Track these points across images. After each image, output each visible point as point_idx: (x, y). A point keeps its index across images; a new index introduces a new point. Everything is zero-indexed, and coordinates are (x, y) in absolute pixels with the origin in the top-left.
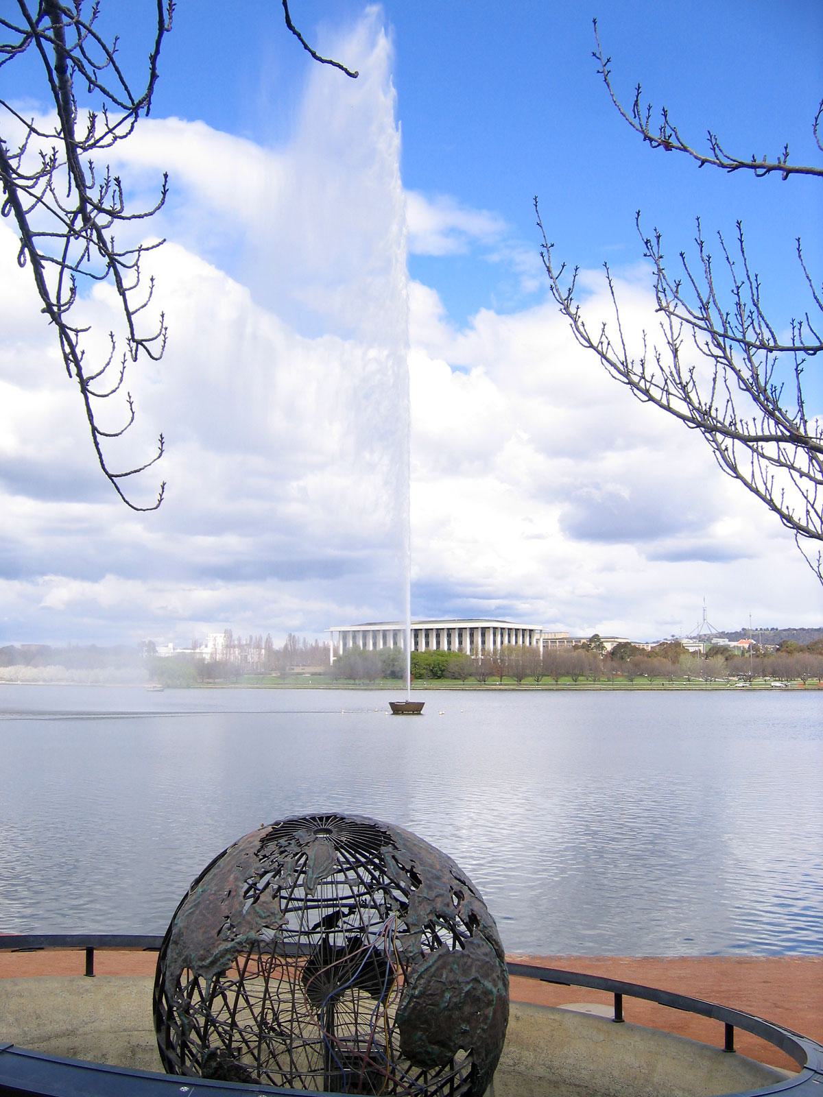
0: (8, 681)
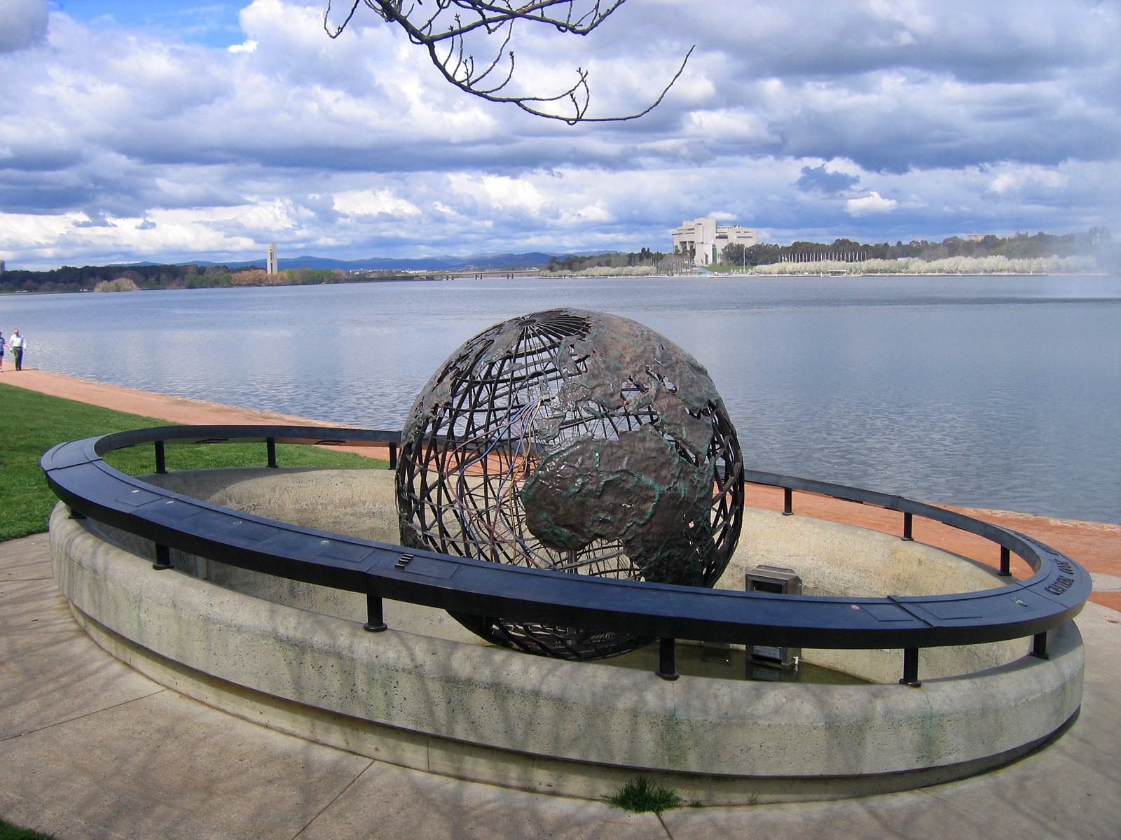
0: (949, 273)
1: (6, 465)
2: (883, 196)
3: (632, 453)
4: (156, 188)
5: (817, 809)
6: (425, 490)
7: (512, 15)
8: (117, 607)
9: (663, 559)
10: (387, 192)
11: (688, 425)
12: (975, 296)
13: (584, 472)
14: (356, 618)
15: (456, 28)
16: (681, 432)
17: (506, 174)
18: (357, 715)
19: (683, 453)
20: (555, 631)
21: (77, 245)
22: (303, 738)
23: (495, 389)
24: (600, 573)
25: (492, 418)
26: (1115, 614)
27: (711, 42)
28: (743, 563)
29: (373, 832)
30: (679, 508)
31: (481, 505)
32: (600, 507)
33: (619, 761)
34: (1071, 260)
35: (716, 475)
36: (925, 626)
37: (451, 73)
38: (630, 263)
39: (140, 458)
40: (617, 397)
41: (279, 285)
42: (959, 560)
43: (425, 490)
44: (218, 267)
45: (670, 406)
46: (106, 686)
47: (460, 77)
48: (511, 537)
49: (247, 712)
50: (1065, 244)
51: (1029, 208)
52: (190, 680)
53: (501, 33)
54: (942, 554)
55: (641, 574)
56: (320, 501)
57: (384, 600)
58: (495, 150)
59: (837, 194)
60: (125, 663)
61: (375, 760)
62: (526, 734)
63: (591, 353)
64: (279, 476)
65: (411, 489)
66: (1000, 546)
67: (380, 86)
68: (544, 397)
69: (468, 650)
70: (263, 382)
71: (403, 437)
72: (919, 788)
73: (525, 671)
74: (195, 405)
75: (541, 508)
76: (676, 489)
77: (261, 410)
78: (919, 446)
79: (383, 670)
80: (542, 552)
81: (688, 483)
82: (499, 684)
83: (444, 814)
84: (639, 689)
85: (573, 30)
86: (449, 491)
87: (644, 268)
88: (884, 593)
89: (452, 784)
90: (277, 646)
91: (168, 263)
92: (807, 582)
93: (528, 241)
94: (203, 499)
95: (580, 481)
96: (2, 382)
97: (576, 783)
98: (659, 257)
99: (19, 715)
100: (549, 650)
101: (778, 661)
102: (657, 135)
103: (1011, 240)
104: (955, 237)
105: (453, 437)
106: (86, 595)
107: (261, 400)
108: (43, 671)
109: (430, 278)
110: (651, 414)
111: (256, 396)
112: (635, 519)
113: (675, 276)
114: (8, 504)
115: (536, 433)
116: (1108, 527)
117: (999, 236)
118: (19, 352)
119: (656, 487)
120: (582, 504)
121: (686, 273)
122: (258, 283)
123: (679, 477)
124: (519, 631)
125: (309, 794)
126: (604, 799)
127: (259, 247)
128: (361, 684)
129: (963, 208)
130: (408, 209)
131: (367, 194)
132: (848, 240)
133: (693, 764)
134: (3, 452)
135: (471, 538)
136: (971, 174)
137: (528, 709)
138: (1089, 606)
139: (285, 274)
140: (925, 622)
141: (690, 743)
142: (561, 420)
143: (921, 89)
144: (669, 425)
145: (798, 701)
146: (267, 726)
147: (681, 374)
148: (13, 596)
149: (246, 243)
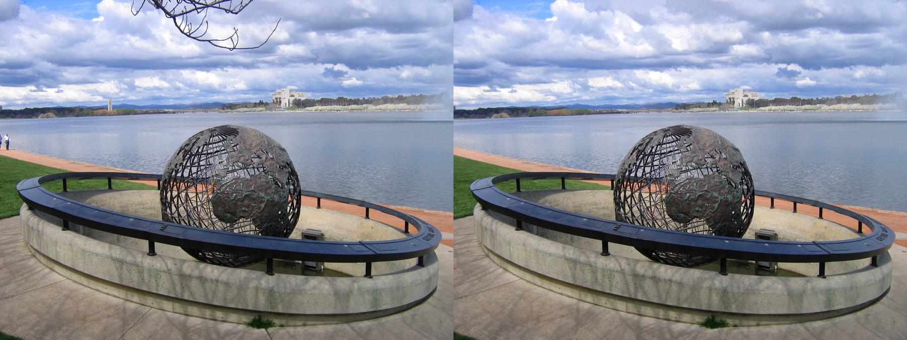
1: (2, 188)
2: (357, 79)
3: (256, 183)
4: (517, 76)
5: (330, 328)
6: (172, 198)
7: (207, 6)
8: (501, 246)
9: (722, 227)
10: (610, 78)
11: (731, 172)
12: (394, 120)
13: (690, 191)
14: (144, 250)
15: (185, 11)
16: (275, 175)
17: (205, 71)
18: (598, 290)
19: (730, 183)
20: (225, 255)
21: (484, 99)
22: (576, 299)
23: (654, 158)
24: (243, 232)
25: (653, 169)
26: (905, 249)
27: (740, 17)
28: (300, 228)
29: (151, 337)
30: (275, 206)
31: (195, 205)
32: (696, 205)
33: (704, 308)
34: (887, 105)
35: (290, 193)
36: (828, 253)
37: (183, 30)
38: (255, 107)
39: (57, 185)
40: (703, 161)
41: (567, 115)
42: (842, 227)
43: (172, 198)
44: (88, 108)
45: (271, 164)
46: (497, 277)
47: (186, 31)
48: (660, 217)
49: (100, 288)
50: (431, 99)
51: (416, 84)
52: (530, 275)
53: (203, 14)
54: (381, 224)
55: (259, 232)
56: (130, 203)
57: (156, 243)
58: (654, 61)
59: (792, 79)
60: (51, 268)
61: (152, 307)
62: (666, 297)
63: (693, 143)
64: (113, 193)
65: (620, 198)
66: (858, 221)
67: (607, 35)
68: (220, 161)
69: (643, 263)
70: (106, 155)
71: (616, 177)
72: (825, 319)
73: (666, 272)
74: (533, 164)
75: (672, 206)
76: (273, 198)
77: (106, 166)
78: (372, 180)
79: (609, 272)
80: (219, 223)
81: (732, 196)
82: (202, 277)
83: (180, 330)
84: (259, 279)
85: (232, 12)
86: (635, 199)
87: (261, 109)
88: (811, 240)
89: (636, 317)
90: (112, 261)
91: (521, 106)
92: (327, 236)
93: (214, 98)
94: (536, 202)
95: (234, 194)
96: (1, 154)
97: (687, 317)
98: (267, 104)
99: (8, 289)
100: (675, 263)
101: (315, 268)
102: (266, 55)
103: (409, 97)
104: (840, 96)
105: (184, 177)
106: (35, 241)
107: (559, 162)
108: (17, 272)
109: (627, 113)
110: (717, 167)
111: (104, 160)
112: (710, 210)
113: (727, 112)
114: (3, 204)
115: (217, 175)
116: (902, 213)
117: (858, 96)
118: (8, 142)
119: (719, 197)
120: (235, 204)
121: (278, 111)
122: (105, 114)
123: (275, 193)
124: (663, 255)
125: (125, 322)
126: (698, 323)
127: (105, 100)
128: (599, 277)
129: (390, 84)
130: (165, 85)
131: (149, 78)
132: (796, 98)
133: (734, 309)
134: (1, 183)
135: (190, 218)
136: (847, 70)
137: (214, 287)
138: (441, 245)
139: (115, 111)
140: (375, 252)
141: (733, 301)
142: (227, 170)
143: (373, 36)
144: (271, 172)
145: (323, 284)
146: (561, 294)
147: (729, 151)
148: (459, 241)
149: (100, 98)
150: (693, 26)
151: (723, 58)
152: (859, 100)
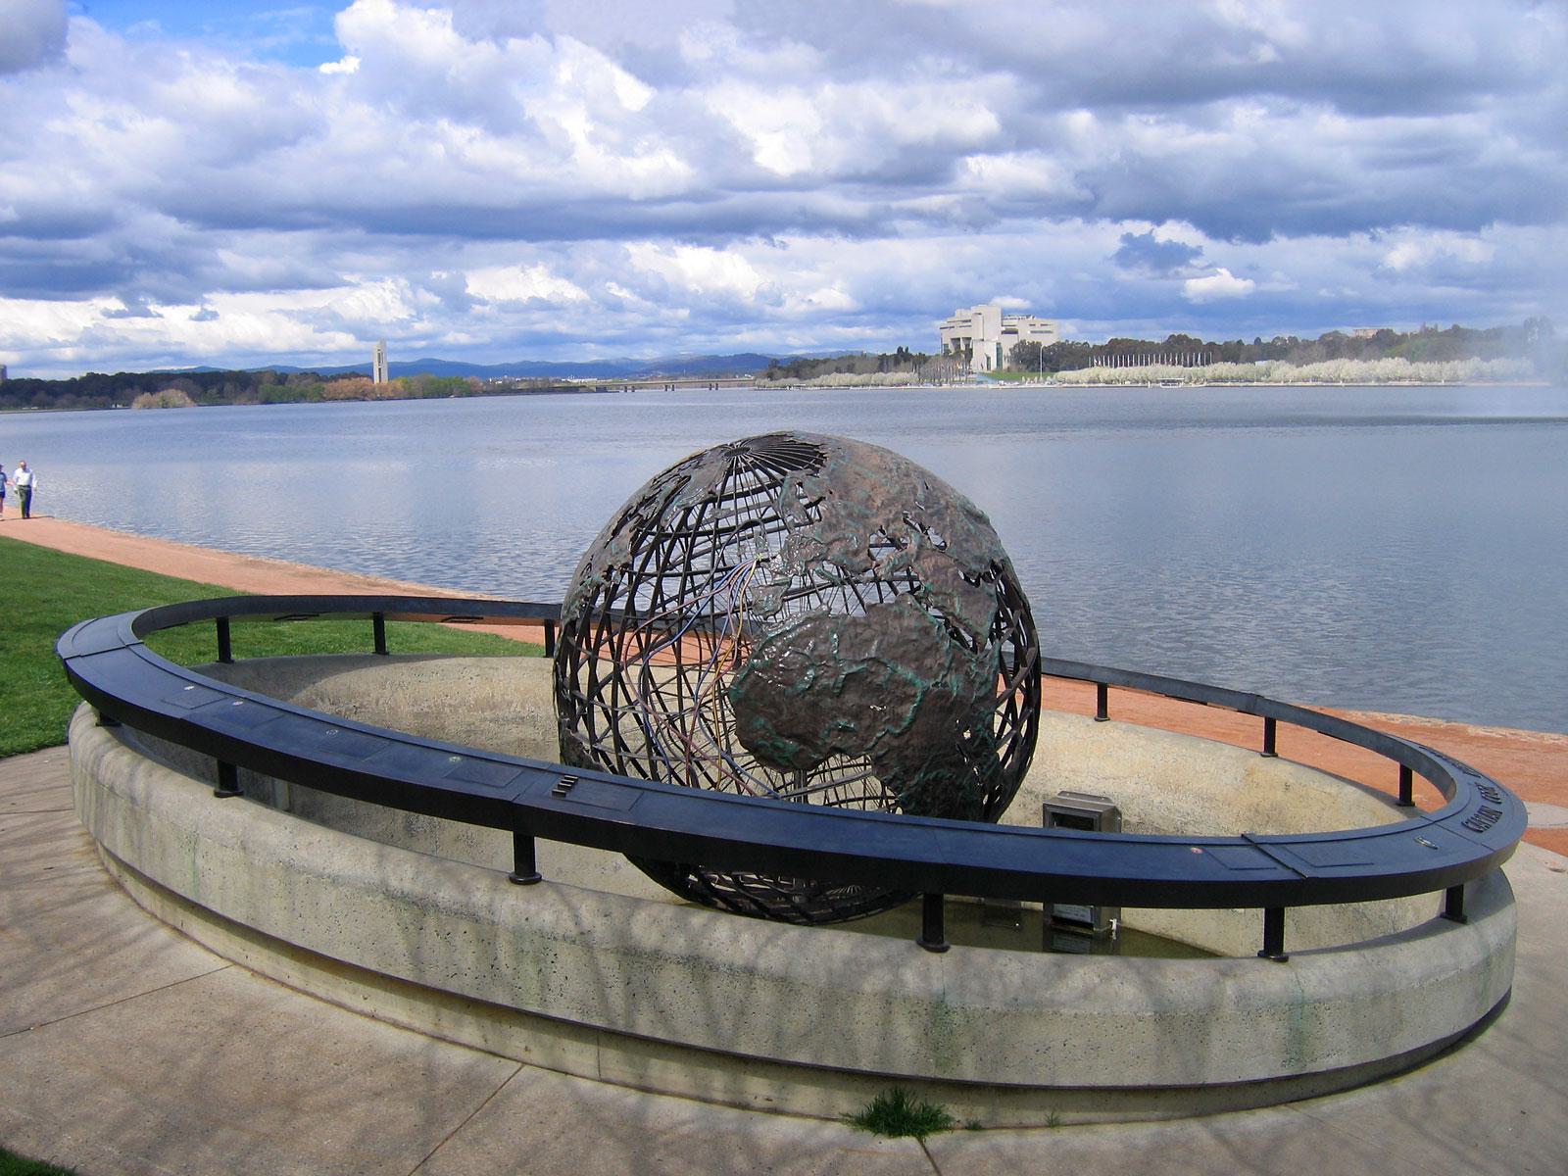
0: (1327, 382)
1: (8, 651)
2: (1236, 275)
3: (884, 634)
4: (219, 264)
5: (1143, 1133)
6: (595, 686)
8: (164, 850)
9: (927, 783)
10: (541, 268)
11: (962, 595)
12: (1364, 414)
13: (817, 661)
14: (497, 865)
16: (953, 605)
17: (708, 244)
18: (499, 1001)
19: (955, 634)
20: (776, 883)
21: (108, 344)
22: (423, 1033)
23: (693, 545)
24: (840, 802)
25: (689, 586)
26: (1559, 860)
27: (992, 58)
28: (1039, 789)
29: (522, 1164)
30: (950, 711)
31: (673, 708)
32: (840, 709)
33: (865, 1065)
34: (1498, 365)
35: (1002, 665)
36: (1294, 877)
38: (881, 369)
39: (196, 641)
40: (863, 555)
41: (390, 399)
42: (1342, 784)
43: (595, 686)
44: (305, 374)
45: (937, 569)
46: (148, 961)
48: (715, 752)
49: (345, 997)
50: (1490, 342)
51: (1440, 292)
52: (266, 952)
54: (1318, 776)
55: (896, 804)
56: (448, 701)
57: (537, 840)
58: (692, 209)
59: (1171, 272)
60: (175, 929)
61: (525, 1063)
62: (736, 1027)
63: (827, 495)
64: (391, 667)
65: (575, 685)
66: (1398, 764)
67: (532, 120)
68: (761, 556)
69: (655, 910)
70: (368, 535)
71: (564, 612)
72: (1285, 1103)
73: (735, 940)
74: (273, 567)
75: (756, 711)
77: (365, 574)
78: (1285, 624)
79: (536, 938)
80: (758, 773)
81: (962, 677)
82: (698, 958)
83: (621, 1140)
84: (894, 964)
86: (628, 688)
87: (901, 376)
88: (1236, 830)
89: (633, 1098)
90: (388, 904)
91: (236, 368)
92: (1129, 815)
93: (739, 337)
94: (284, 699)
95: (811, 673)
97: (806, 1096)
98: (922, 360)
99: (27, 1000)
100: (768, 910)
101: (1089, 926)
102: (919, 189)
103: (1414, 336)
104: (1336, 332)
105: (634, 612)
106: (120, 833)
107: (366, 560)
108: (60, 940)
109: (601, 390)
110: (911, 579)
111: (358, 554)
112: (888, 727)
113: (945, 386)
114: (12, 706)
115: (749, 606)
116: (1550, 738)
117: (1397, 330)
118: (26, 493)
119: (918, 681)
120: (814, 705)
121: (960, 382)
122: (361, 396)
123: (949, 668)
124: (726, 883)
125: (432, 1112)
126: (845, 1119)
127: (363, 345)
128: (505, 958)
129: (1347, 292)
130: (571, 292)
131: (513, 271)
132: (1185, 336)
133: (969, 1070)
134: (4, 633)
135: (659, 754)
136: (1359, 243)
137: (739, 992)
138: (1523, 848)
139: (399, 384)
140: (1294, 870)
141: (965, 1040)
142: (784, 588)
143: (1289, 124)
144: (935, 594)
145: (1116, 982)
146: (373, 1017)
147: (952, 524)
148: (19, 834)
149: (344, 340)
150: (829, 91)
151: (933, 201)
152: (1404, 346)
